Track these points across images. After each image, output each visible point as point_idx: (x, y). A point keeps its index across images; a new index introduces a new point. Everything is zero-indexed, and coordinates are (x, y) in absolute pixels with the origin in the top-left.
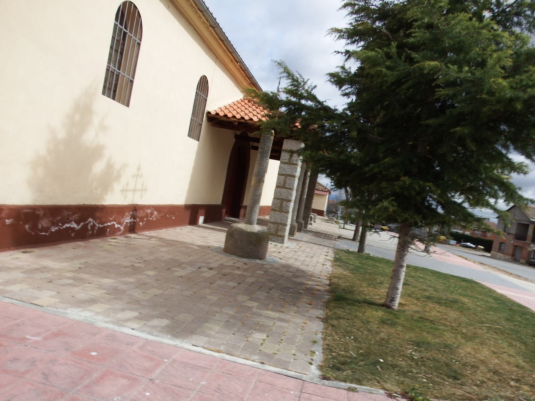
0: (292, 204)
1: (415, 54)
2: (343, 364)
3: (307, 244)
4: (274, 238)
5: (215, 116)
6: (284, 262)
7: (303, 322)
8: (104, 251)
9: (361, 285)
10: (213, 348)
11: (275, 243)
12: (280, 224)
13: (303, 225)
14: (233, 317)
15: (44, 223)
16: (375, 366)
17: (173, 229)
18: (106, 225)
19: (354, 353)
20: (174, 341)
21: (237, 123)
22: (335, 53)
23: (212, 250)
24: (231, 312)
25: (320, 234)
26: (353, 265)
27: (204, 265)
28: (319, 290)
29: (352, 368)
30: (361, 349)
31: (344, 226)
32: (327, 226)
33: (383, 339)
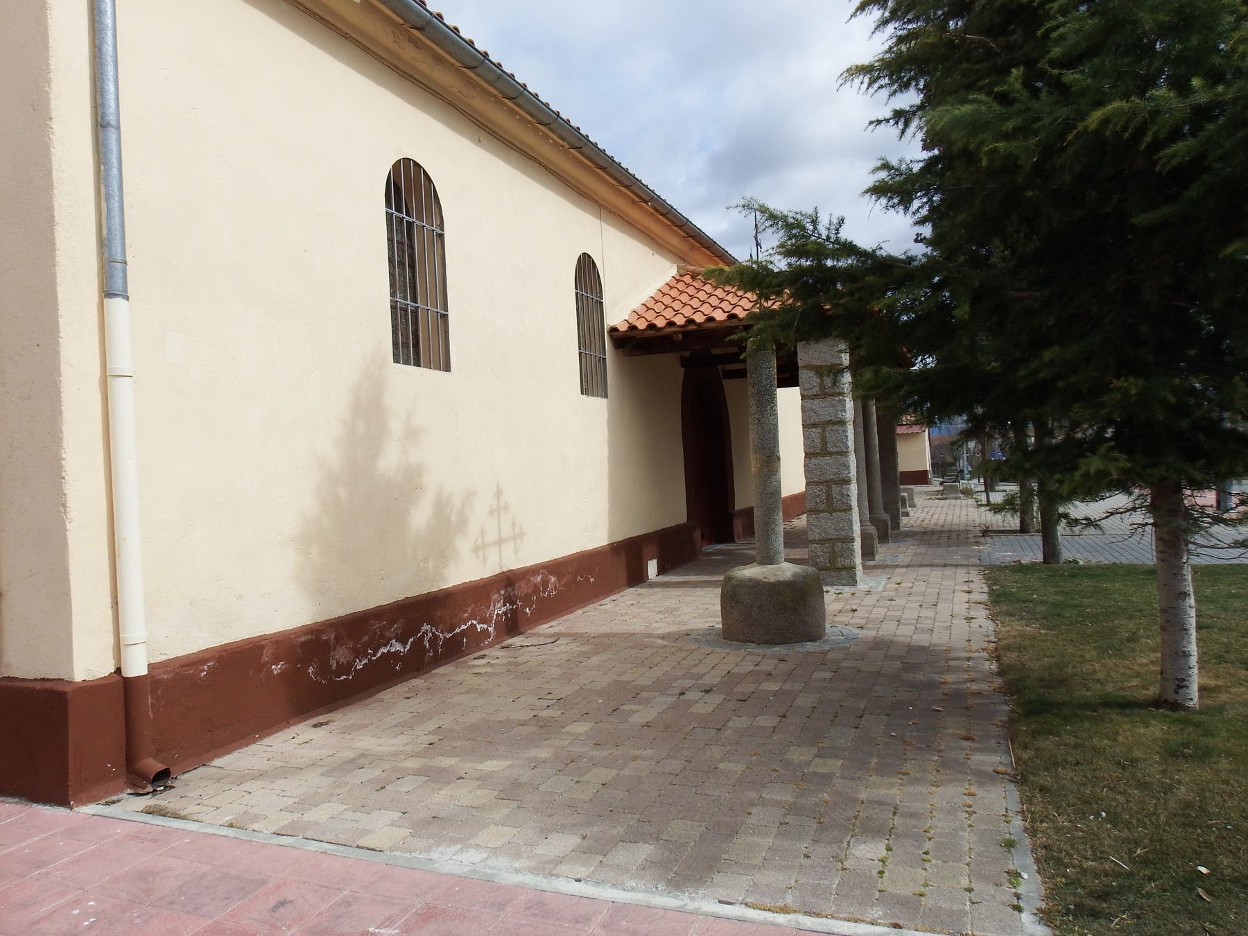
0: (853, 487)
1: (1072, 73)
2: (1103, 896)
3: (912, 574)
4: (831, 576)
5: (629, 333)
6: (869, 634)
7: (966, 792)
8: (467, 692)
9: (1081, 656)
10: (767, 902)
11: (835, 587)
12: (838, 540)
13: (889, 523)
14: (793, 809)
15: (340, 655)
16: (1192, 890)
17: (596, 605)
18: (458, 630)
19: (1121, 859)
20: (676, 897)
21: (680, 336)
22: (872, 127)
23: (696, 640)
24: (786, 796)
25: (935, 537)
26: (1042, 603)
27: (688, 683)
28: (979, 694)
29: (1131, 907)
30: (1137, 843)
31: (988, 498)
32: (945, 510)
33: (1188, 805)
